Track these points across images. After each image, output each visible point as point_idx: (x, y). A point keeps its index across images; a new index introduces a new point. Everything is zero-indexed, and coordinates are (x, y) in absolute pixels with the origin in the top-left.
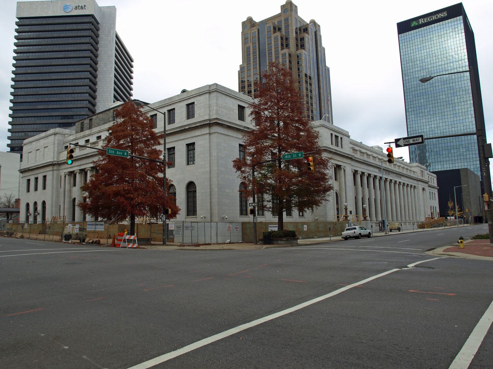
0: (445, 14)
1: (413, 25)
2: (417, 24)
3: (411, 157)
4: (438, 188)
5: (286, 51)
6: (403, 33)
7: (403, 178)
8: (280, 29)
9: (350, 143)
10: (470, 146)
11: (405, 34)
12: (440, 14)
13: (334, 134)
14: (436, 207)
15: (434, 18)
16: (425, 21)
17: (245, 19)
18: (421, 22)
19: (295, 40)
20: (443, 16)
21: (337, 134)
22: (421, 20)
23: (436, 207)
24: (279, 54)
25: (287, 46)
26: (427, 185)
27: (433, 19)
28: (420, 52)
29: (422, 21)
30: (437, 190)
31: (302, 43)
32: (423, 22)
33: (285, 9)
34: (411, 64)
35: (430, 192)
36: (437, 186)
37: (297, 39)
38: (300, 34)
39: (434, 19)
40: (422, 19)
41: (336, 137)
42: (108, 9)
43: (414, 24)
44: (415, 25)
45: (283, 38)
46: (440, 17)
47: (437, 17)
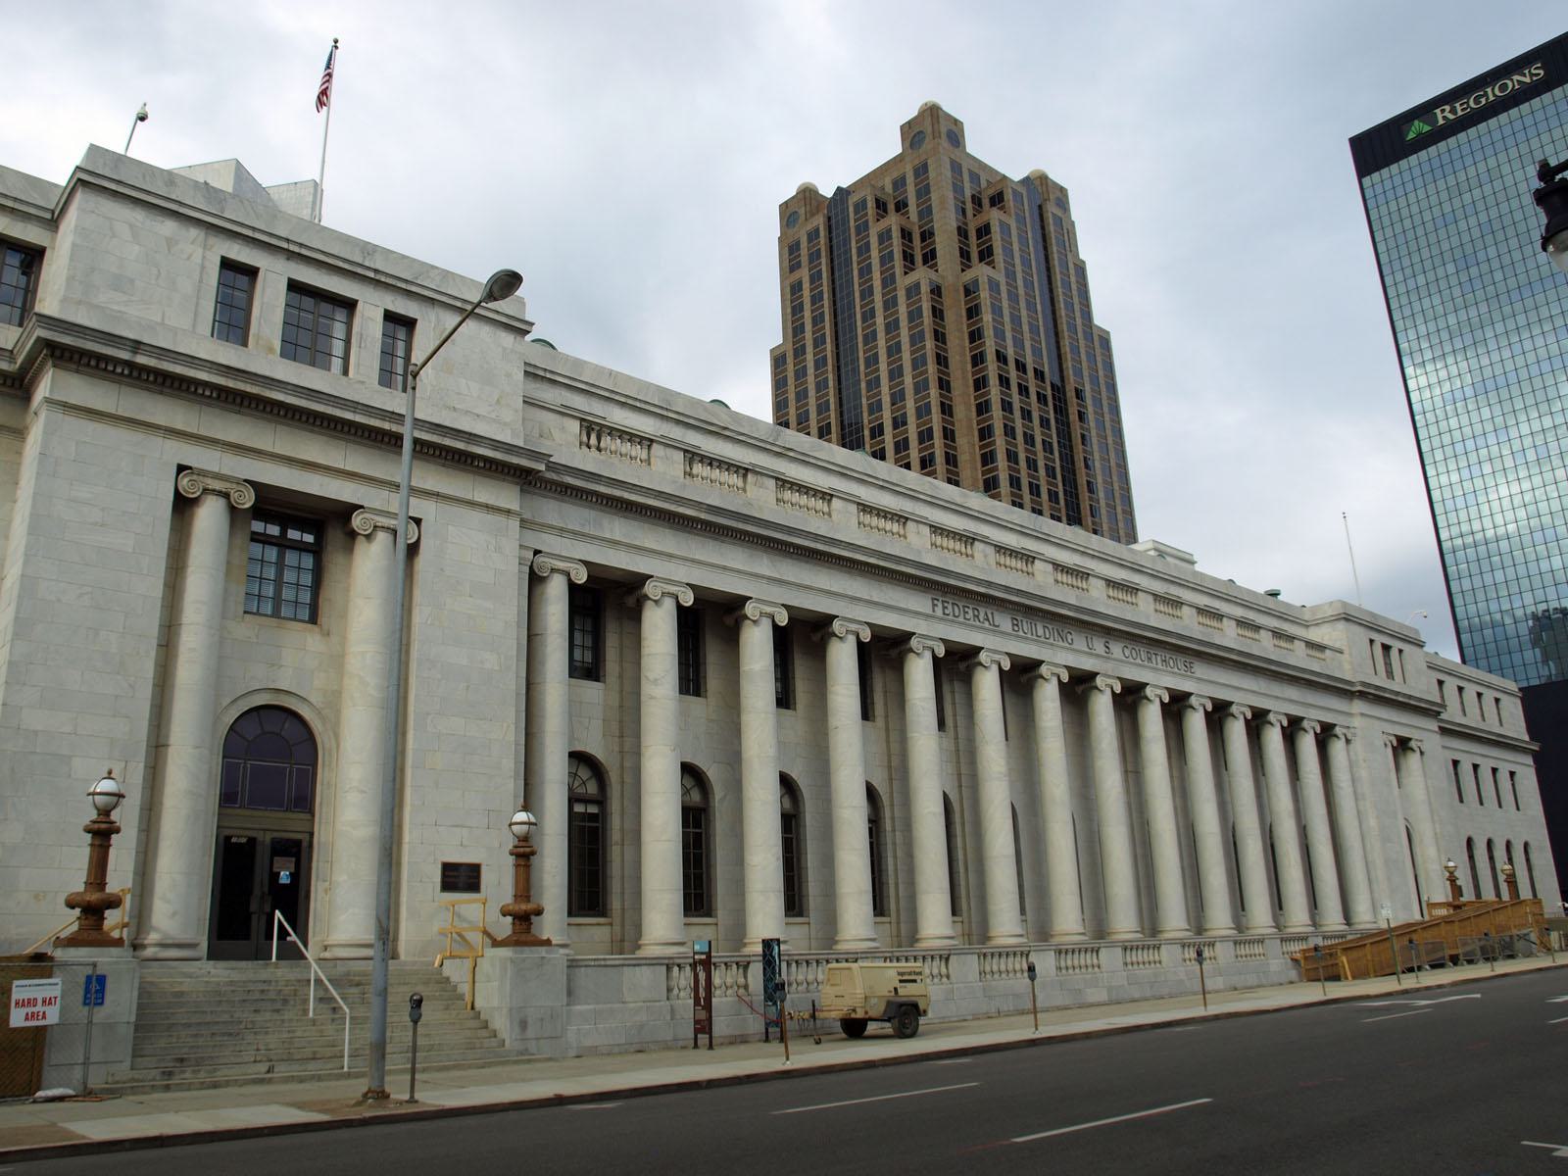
0: (1538, 71)
1: (1411, 136)
2: (1427, 128)
3: (216, 165)
4: (1535, 747)
5: (922, 275)
6: (1378, 169)
7: (1201, 670)
8: (901, 206)
9: (1429, 667)
10: (1499, 420)
11: (1385, 172)
12: (1516, 78)
13: (1380, 639)
14: (1526, 845)
15: (1493, 93)
16: (1460, 113)
17: (791, 192)
18: (1444, 118)
19: (956, 238)
20: (1527, 80)
21: (1388, 641)
22: (1443, 111)
23: (1526, 845)
24: (895, 289)
25: (930, 257)
26: (1433, 725)
27: (1487, 99)
28: (1452, 228)
29: (1446, 114)
30: (1529, 760)
31: (984, 243)
32: (1451, 117)
33: (915, 136)
34: (1421, 280)
35: (1455, 763)
36: (1527, 738)
37: (962, 232)
38: (975, 215)
39: (1491, 98)
40: (1447, 108)
41: (1386, 648)
42: (293, 192)
43: (1419, 127)
44: (1420, 134)
45: (910, 234)
46: (1517, 87)
47: (1503, 87)
